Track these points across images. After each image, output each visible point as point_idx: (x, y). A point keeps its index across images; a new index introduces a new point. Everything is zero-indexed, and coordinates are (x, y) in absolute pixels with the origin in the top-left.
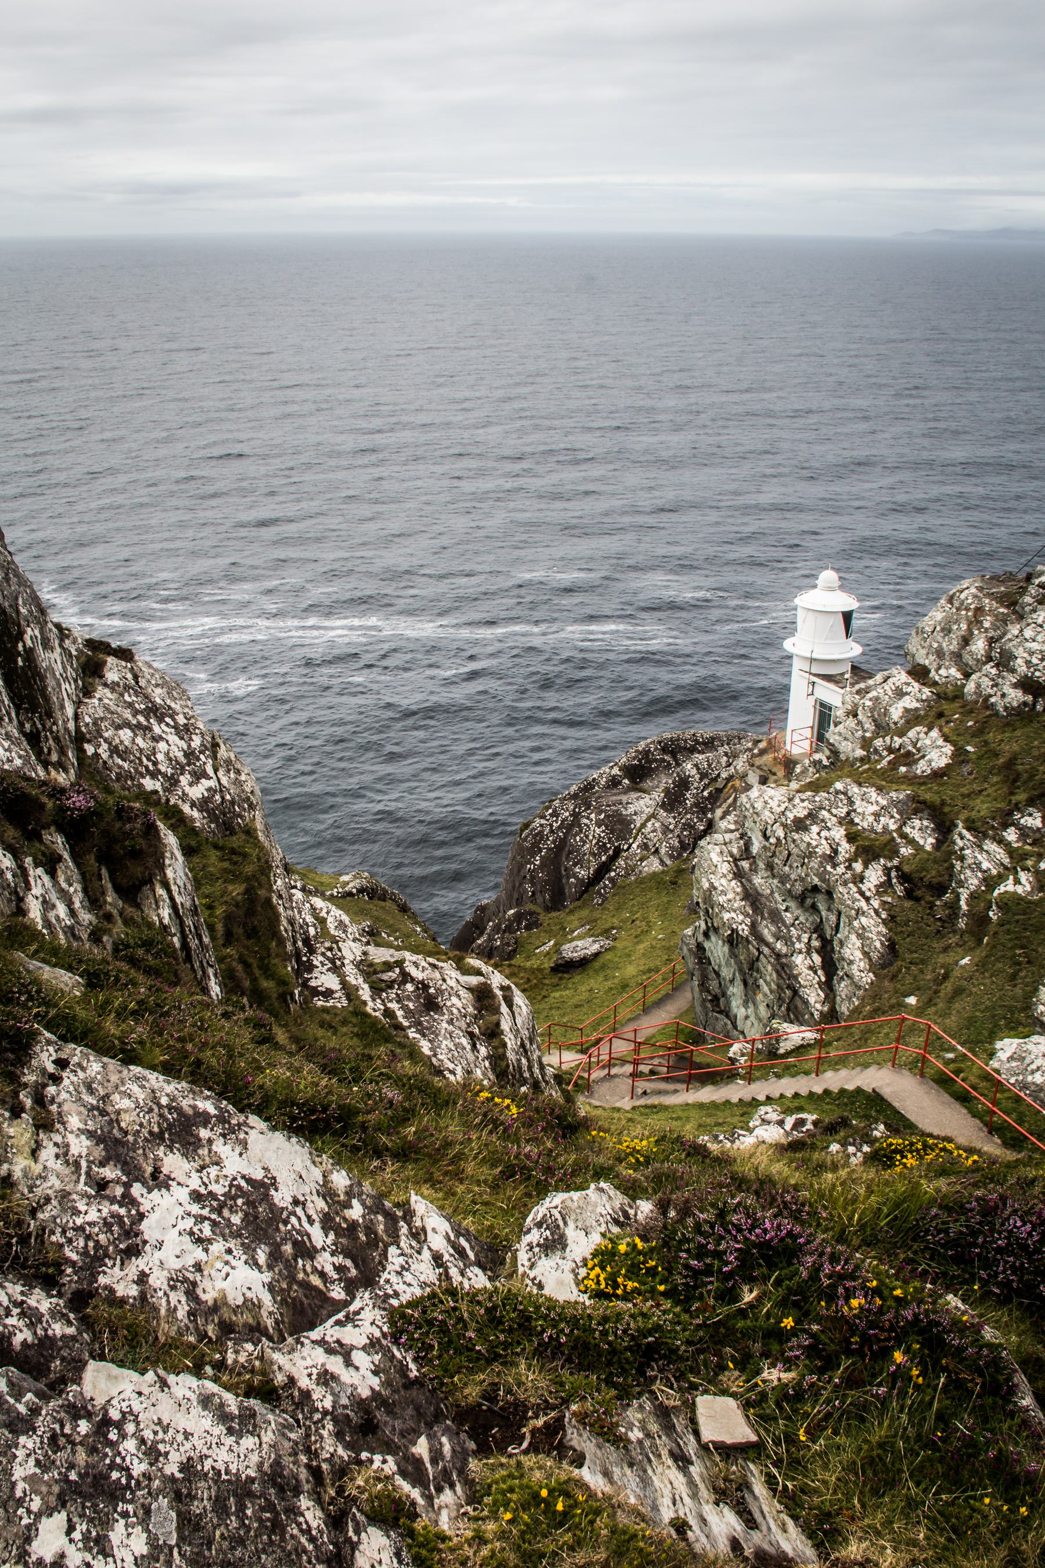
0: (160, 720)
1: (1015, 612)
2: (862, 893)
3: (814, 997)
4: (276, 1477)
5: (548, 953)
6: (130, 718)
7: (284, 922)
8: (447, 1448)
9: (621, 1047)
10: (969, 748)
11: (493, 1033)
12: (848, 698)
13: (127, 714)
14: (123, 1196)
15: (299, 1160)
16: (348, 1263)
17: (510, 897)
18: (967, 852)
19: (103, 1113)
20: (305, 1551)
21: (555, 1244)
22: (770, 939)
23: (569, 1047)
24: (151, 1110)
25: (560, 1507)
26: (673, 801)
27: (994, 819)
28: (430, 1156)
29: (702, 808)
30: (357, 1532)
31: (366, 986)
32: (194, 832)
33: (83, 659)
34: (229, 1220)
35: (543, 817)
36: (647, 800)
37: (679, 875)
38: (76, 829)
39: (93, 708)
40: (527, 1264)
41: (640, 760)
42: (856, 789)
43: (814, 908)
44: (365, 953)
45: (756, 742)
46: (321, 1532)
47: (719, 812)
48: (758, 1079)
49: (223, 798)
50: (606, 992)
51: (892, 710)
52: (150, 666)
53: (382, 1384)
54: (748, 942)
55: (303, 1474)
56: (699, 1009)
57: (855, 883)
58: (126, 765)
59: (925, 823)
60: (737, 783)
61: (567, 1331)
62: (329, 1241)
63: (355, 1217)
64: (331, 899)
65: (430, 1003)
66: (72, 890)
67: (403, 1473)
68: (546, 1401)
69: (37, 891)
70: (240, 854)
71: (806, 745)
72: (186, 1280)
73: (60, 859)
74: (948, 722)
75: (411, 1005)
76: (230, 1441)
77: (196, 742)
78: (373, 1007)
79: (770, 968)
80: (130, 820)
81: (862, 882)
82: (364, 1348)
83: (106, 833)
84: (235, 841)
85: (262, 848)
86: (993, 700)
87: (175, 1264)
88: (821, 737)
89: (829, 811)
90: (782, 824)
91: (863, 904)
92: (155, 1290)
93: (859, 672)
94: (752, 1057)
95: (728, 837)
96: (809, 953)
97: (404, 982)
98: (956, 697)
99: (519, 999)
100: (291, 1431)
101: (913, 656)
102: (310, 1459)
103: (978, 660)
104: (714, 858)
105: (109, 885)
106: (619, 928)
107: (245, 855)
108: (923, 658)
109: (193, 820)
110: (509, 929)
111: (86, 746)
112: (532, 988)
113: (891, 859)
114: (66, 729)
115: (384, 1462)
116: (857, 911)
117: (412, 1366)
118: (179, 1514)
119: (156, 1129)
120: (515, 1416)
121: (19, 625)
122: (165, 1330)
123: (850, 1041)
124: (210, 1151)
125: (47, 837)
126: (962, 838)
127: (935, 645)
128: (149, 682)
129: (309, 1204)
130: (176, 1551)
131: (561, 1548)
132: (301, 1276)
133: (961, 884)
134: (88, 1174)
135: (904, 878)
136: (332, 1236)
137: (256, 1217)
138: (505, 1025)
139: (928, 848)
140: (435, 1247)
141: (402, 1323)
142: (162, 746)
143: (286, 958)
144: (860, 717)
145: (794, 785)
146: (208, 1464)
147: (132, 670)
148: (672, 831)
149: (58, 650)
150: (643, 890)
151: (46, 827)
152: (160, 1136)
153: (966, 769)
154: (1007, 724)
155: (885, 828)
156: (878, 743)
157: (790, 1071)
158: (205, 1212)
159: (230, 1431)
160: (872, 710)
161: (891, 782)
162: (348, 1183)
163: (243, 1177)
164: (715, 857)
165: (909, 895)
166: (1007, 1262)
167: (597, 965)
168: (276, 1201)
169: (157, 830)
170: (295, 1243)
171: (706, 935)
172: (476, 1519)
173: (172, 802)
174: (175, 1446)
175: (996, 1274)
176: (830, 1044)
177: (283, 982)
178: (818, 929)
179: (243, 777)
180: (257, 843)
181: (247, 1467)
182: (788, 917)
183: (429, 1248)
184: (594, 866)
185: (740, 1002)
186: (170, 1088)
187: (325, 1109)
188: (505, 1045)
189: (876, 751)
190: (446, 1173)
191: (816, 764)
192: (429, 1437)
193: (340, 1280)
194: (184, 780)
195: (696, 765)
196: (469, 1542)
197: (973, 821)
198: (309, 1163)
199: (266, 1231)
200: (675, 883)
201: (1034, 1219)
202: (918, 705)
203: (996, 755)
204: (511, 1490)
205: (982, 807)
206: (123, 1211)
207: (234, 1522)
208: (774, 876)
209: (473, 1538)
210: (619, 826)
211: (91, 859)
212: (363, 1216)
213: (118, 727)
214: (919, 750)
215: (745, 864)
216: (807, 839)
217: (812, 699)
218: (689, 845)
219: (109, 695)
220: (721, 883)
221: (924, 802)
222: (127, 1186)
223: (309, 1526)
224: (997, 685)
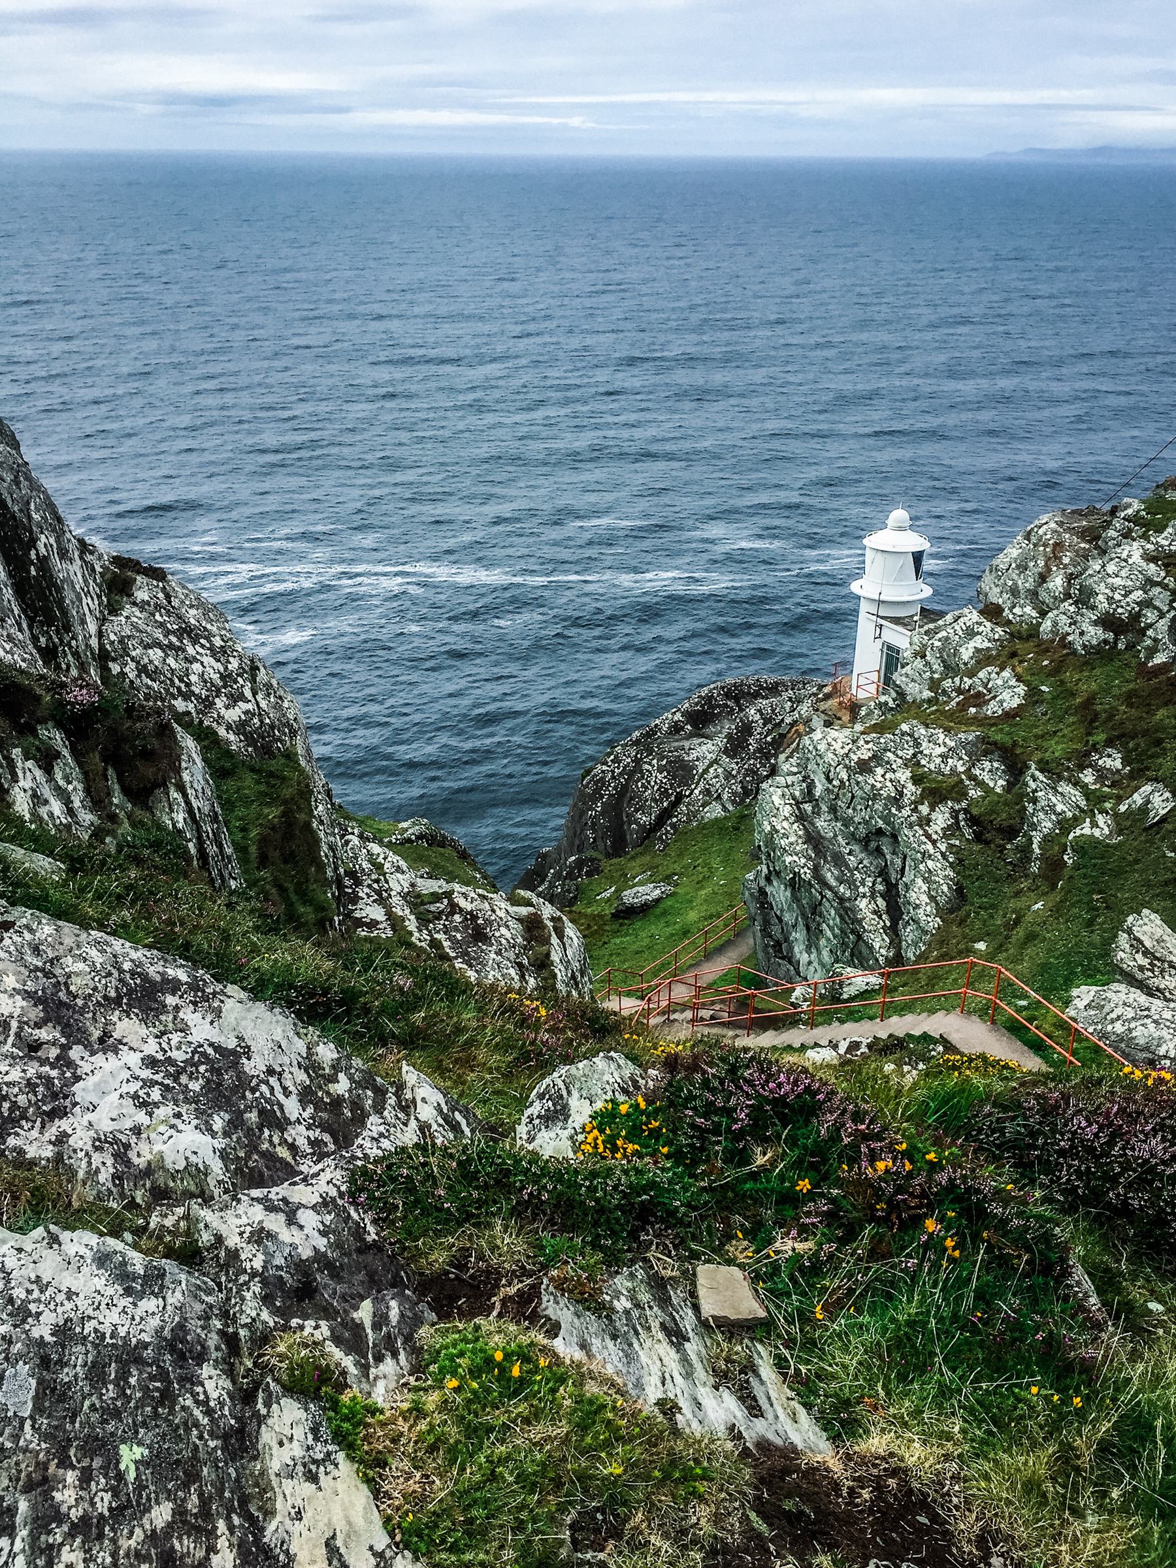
0: (195, 642)
1: (1097, 547)
2: (928, 837)
3: (879, 943)
4: (180, 1348)
5: (609, 899)
6: (161, 637)
7: (325, 848)
8: (394, 1314)
9: (681, 993)
10: (1043, 688)
11: (543, 965)
12: (916, 640)
13: (158, 634)
14: (58, 1058)
15: (279, 1030)
16: (327, 1138)
17: (571, 844)
19: (48, 975)
20: (196, 1424)
21: (558, 1114)
22: (833, 883)
23: (629, 994)
24: (109, 974)
25: (516, 1372)
26: (735, 746)
27: (1069, 760)
28: (439, 1042)
30: (268, 1405)
31: (412, 917)
32: (229, 754)
33: (108, 576)
34: (186, 1086)
35: (605, 763)
37: (742, 820)
38: (79, 726)
39: (118, 626)
40: (525, 1137)
42: (923, 731)
43: (878, 851)
44: (413, 885)
45: (821, 687)
46: (222, 1404)
47: (782, 757)
48: (821, 1024)
49: (262, 722)
50: (667, 938)
51: (962, 650)
52: (184, 587)
53: (330, 1245)
54: (811, 886)
55: (213, 1340)
56: (760, 955)
57: (921, 826)
58: (155, 685)
59: (996, 765)
60: (801, 728)
61: (550, 1187)
62: (306, 1115)
63: (340, 1092)
64: (390, 845)
65: (478, 933)
66: (70, 787)
67: (337, 1340)
68: (523, 1267)
69: (25, 783)
70: (278, 777)
71: (873, 689)
72: (116, 1141)
73: (58, 755)
74: (1021, 662)
75: (459, 936)
76: (126, 1301)
77: (234, 664)
78: (420, 938)
79: (833, 912)
80: (140, 718)
82: (314, 1208)
83: (112, 731)
84: (274, 765)
85: (302, 771)
86: (1070, 638)
87: (106, 1126)
88: (888, 681)
90: (846, 766)
91: (929, 847)
92: (75, 1151)
93: (928, 614)
94: (814, 1002)
95: (790, 779)
96: (873, 897)
97: (452, 913)
98: (1030, 636)
99: (570, 931)
100: (209, 1294)
101: (986, 595)
102: (226, 1325)
103: (1055, 598)
104: (776, 802)
105: (116, 787)
106: (680, 875)
107: (284, 779)
108: (996, 596)
109: (228, 743)
110: (570, 876)
111: (111, 664)
112: (592, 934)
113: (959, 802)
114: (88, 646)
115: (317, 1327)
116: (924, 854)
117: (371, 1228)
118: (40, 1383)
119: (113, 994)
120: (486, 1284)
121: (31, 532)
122: (83, 1194)
123: (916, 986)
124: (175, 1018)
125: (43, 732)
126: (1035, 780)
128: (182, 602)
129: (286, 1075)
130: (28, 1423)
131: (514, 1421)
132: (265, 1146)
133: (1033, 826)
134: (18, 1035)
135: (973, 821)
136: (310, 1110)
137: (219, 1084)
138: (555, 957)
139: (999, 790)
140: (422, 1117)
141: (361, 1183)
142: (196, 667)
143: (327, 883)
145: (858, 727)
146: (89, 1327)
147: (164, 589)
148: (734, 777)
149: (79, 562)
150: (705, 836)
151: (42, 721)
152: (118, 1001)
153: (1040, 710)
154: (1086, 663)
155: (953, 770)
156: (947, 684)
157: (853, 1016)
158: (158, 1077)
159: (128, 1292)
160: (941, 650)
161: (960, 723)
162: (336, 1056)
163: (211, 1045)
164: (777, 800)
165: (978, 838)
166: (1070, 1166)
167: (658, 911)
168: (247, 1069)
169: (172, 730)
170: (262, 1112)
171: (768, 879)
172: (417, 1389)
173: (206, 723)
174: (52, 1307)
175: (1059, 1178)
176: (895, 989)
177: (321, 908)
178: (883, 873)
179: (286, 704)
180: (297, 767)
181: (142, 1331)
182: (852, 861)
183: (417, 1119)
184: (656, 811)
185: (802, 947)
186: (134, 955)
187: (325, 992)
188: (555, 976)
189: (944, 692)
190: (456, 1061)
191: (882, 706)
192: (376, 1301)
193: (313, 1154)
194: (220, 703)
195: (759, 711)
196: (405, 1416)
197: (1047, 763)
198: (291, 1034)
199: (228, 1099)
200: (737, 829)
201: (1101, 1119)
203: (1073, 695)
204: (462, 1354)
205: (1057, 749)
206: (54, 1073)
207: (111, 1392)
208: (837, 820)
209: (410, 1410)
210: (681, 771)
211: (96, 758)
212: (350, 1091)
213: (147, 647)
214: (989, 691)
215: (808, 807)
216: (871, 781)
217: (879, 642)
218: (750, 793)
219: (138, 614)
220: (782, 826)
221: (995, 743)
222: (65, 1048)
223: (207, 1397)
224: (1075, 623)
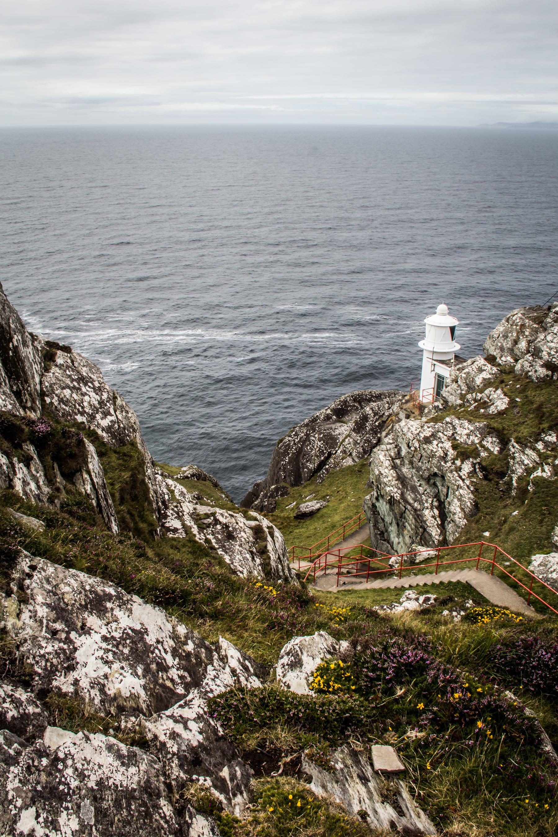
0: (86, 384)
1: (542, 327)
2: (460, 477)
3: (435, 532)
4: (147, 788)
5: (293, 509)
6: (70, 383)
7: (152, 492)
8: (239, 773)
9: (332, 559)
10: (518, 399)
11: (263, 552)
12: (453, 373)
13: (68, 381)
14: (66, 638)
15: (159, 619)
16: (186, 674)
17: (272, 479)
18: (516, 455)
19: (55, 594)
20: (163, 828)
21: (296, 664)
22: (411, 501)
23: (304, 559)
24: (80, 593)
25: (299, 804)
26: (359, 428)
27: (531, 437)
28: (230, 617)
29: (375, 431)
30: (191, 818)
31: (195, 527)
32: (103, 444)
33: (44, 352)
34: (122, 651)
35: (290, 436)
36: (345, 427)
37: (363, 467)
38: (41, 442)
39: (50, 378)
40: (281, 675)
41: (342, 406)
42: (457, 421)
43: (435, 485)
44: (195, 509)
45: (404, 396)
46: (171, 818)
47: (384, 434)
48: (405, 576)
49: (119, 426)
50: (324, 530)
51: (476, 379)
52: (80, 356)
53: (204, 739)
54: (400, 503)
55: (162, 787)
56: (373, 539)
57: (456, 471)
58: (67, 408)
59: (494, 439)
60: (394, 418)
61: (303, 710)
62: (176, 663)
63: (190, 650)
64: (177, 480)
65: (230, 536)
66: (38, 475)
67: (215, 786)
68: (292, 748)
69: (20, 475)
70: (128, 456)
71: (431, 398)
72: (99, 683)
73: (32, 458)
74: (506, 386)
75: (219, 537)
76: (123, 769)
77: (105, 396)
78: (199, 538)
79: (411, 517)
80: (69, 438)
81: (460, 471)
82: (194, 720)
83: (56, 445)
84: (126, 449)
85: (140, 453)
86: (530, 374)
87: (94, 675)
88: (438, 394)
89: (443, 433)
90: (418, 440)
91: (461, 482)
92: (83, 689)
93: (458, 359)
94: (401, 564)
95: (389, 447)
96: (432, 508)
97: (216, 524)
98: (510, 372)
99: (277, 533)
100: (155, 764)
101: (488, 350)
102: (166, 779)
103: (522, 353)
104: (381, 458)
105: (58, 473)
106: (330, 496)
107: (131, 457)
108: (493, 351)
109: (103, 438)
110: (272, 496)
111: (46, 398)
112: (284, 527)
113: (476, 459)
114: (35, 389)
115: (205, 780)
116: (458, 486)
117: (220, 729)
118: (96, 808)
119: (83, 603)
120: (275, 756)
121: (10, 334)
122: (88, 710)
123: (454, 555)
124: (112, 614)
125: (25, 447)
126: (514, 447)
127: (499, 344)
128: (79, 364)
129: (165, 643)
130: (94, 828)
131: (300, 827)
132: (161, 681)
133: (513, 472)
134: (47, 627)
135: (483, 468)
136: (177, 660)
137: (137, 650)
138: (270, 547)
139: (496, 453)
140: (232, 666)
141: (214, 706)
142: (86, 398)
143: (153, 511)
144: (459, 383)
145: (424, 419)
146: (111, 781)
147: (70, 357)
148: (359, 444)
149: (31, 347)
150: (343, 475)
151: (25, 441)
152: (86, 606)
153: (516, 410)
154: (538, 387)
155: (473, 442)
156: (469, 396)
157: (422, 572)
158: (110, 647)
159: (123, 764)
160: (466, 379)
161: (476, 417)
162: (186, 631)
163: (130, 628)
164: (382, 458)
165: (486, 478)
166: (538, 674)
167: (319, 515)
168: (147, 641)
169: (84, 443)
170: (158, 664)
171: (377, 499)
172: (254, 811)
173: (92, 428)
174: (93, 772)
175: (532, 680)
176: (443, 557)
177: (151, 524)
178: (437, 496)
179: (130, 415)
180: (137, 450)
181: (132, 783)
182: (421, 490)
183: (229, 666)
184: (317, 462)
185: (395, 535)
186: (91, 581)
187: (173, 592)
188: (269, 558)
189: (468, 401)
190: (238, 626)
191: (436, 408)
192: (229, 767)
193: (182, 683)
194: (99, 416)
195: (372, 409)
196: (251, 823)
197: (520, 438)
198: (165, 621)
199: (142, 657)
200: (360, 471)
201: (552, 650)
202: (490, 376)
203: (532, 403)
204: (273, 795)
205: (525, 431)
206: (65, 647)
207: (125, 813)
208: (413, 468)
209: (253, 821)
210: (331, 441)
211: (49, 459)
212: (194, 649)
213: (63, 388)
214: (490, 400)
215: (398, 461)
216: (431, 448)
217: (434, 373)
218: (368, 451)
219: (58, 371)
220: (385, 471)
221: (493, 428)
222: (68, 633)
223: (165, 815)
224: (532, 366)
